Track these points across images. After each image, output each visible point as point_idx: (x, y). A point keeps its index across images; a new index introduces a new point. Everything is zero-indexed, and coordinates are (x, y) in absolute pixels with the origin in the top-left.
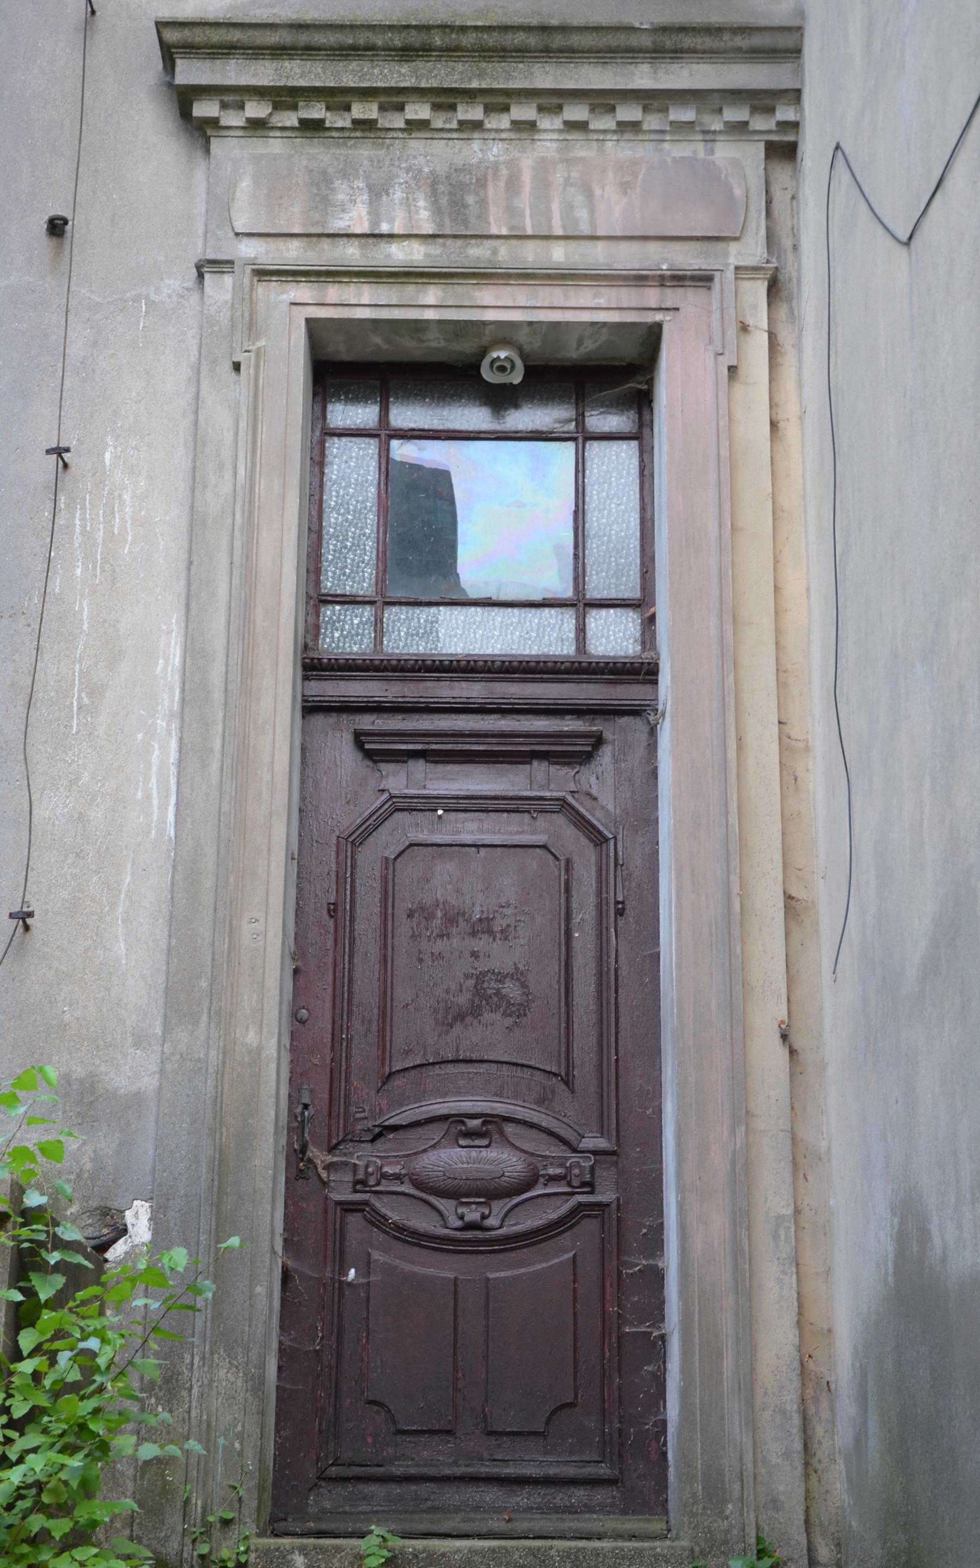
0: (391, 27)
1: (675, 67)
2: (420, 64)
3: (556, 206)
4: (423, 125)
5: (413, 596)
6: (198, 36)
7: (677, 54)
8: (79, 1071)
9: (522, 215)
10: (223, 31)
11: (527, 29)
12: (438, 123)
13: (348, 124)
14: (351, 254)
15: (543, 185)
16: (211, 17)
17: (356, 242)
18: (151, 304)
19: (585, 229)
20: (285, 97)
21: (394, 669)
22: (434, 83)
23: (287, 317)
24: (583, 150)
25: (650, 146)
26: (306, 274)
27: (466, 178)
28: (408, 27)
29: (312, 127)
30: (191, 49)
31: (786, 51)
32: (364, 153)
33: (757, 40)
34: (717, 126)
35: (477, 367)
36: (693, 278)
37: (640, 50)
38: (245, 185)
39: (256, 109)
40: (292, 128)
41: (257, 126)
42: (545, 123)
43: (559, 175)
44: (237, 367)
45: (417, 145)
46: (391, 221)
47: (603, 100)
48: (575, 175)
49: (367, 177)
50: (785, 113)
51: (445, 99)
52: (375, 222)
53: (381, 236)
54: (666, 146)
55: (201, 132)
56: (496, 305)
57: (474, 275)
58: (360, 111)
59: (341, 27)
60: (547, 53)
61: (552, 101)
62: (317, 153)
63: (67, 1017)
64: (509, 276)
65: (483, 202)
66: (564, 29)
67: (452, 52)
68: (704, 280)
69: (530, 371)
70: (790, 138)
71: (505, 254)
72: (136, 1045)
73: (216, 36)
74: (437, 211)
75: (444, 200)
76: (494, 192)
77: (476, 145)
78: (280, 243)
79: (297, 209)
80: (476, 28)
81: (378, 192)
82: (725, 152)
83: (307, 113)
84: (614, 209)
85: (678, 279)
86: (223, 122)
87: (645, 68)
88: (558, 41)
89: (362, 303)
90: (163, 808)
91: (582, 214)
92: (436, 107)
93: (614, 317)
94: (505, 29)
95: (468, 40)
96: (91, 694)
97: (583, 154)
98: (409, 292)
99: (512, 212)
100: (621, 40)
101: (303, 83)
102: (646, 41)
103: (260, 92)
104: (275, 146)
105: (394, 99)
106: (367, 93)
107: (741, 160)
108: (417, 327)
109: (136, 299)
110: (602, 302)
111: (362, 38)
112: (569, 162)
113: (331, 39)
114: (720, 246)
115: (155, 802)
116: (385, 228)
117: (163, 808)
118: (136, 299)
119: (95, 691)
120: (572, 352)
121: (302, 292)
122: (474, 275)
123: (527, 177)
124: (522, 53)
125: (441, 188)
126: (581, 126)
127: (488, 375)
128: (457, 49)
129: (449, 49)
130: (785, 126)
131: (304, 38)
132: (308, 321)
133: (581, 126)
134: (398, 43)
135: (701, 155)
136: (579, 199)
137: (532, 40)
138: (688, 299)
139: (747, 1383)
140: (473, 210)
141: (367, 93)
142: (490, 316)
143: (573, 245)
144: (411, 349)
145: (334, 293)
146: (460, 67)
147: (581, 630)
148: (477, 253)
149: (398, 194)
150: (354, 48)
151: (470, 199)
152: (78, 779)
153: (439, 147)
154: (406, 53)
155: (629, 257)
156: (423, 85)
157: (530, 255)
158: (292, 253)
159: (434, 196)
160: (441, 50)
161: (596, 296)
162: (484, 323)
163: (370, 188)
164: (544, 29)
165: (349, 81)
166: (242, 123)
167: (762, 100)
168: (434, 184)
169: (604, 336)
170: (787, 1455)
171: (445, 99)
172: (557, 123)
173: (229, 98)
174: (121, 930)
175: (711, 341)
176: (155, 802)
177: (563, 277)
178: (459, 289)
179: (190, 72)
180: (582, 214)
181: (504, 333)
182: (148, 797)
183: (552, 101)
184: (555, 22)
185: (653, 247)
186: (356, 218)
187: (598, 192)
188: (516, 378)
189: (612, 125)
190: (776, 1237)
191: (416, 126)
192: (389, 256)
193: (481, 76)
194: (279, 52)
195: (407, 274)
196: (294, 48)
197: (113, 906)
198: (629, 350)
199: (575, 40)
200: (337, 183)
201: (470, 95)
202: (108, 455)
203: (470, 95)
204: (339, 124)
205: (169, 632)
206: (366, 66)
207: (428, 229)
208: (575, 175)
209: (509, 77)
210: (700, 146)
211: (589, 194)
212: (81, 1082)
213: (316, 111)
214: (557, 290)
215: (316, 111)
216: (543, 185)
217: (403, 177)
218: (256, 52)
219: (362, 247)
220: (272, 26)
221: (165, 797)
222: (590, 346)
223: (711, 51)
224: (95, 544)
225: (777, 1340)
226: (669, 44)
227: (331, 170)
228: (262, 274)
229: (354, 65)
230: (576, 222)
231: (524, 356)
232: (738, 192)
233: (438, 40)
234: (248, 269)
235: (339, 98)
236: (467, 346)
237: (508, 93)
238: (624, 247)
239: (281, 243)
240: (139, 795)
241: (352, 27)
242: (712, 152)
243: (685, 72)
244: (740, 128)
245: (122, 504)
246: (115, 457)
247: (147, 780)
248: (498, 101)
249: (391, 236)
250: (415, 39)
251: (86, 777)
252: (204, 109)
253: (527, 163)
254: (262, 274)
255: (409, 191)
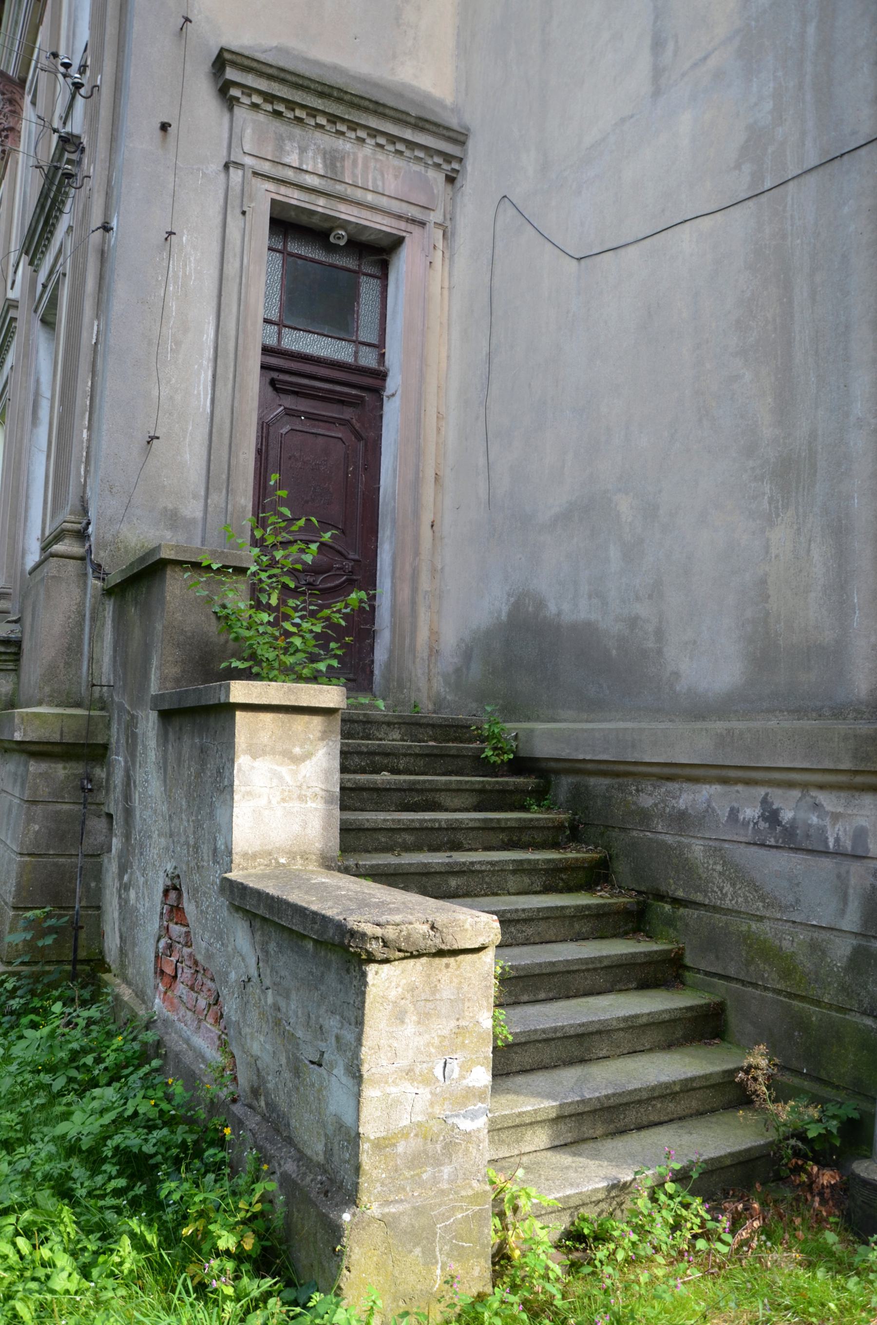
0: (318, 82)
1: (420, 134)
2: (326, 101)
3: (370, 177)
4: (322, 127)
5: (294, 325)
6: (239, 60)
7: (422, 129)
8: (170, 506)
9: (357, 177)
10: (250, 61)
11: (370, 101)
12: (328, 128)
13: (292, 117)
14: (290, 174)
15: (366, 167)
16: (233, 49)
17: (292, 170)
18: (204, 173)
19: (380, 190)
20: (270, 98)
21: (289, 355)
22: (331, 111)
23: (263, 196)
24: (381, 156)
25: (405, 162)
26: (273, 179)
27: (337, 155)
28: (325, 84)
29: (277, 114)
30: (234, 64)
31: (460, 142)
32: (297, 131)
33: (451, 134)
34: (430, 162)
35: (328, 236)
36: (419, 222)
37: (410, 123)
38: (249, 131)
39: (256, 99)
40: (269, 112)
41: (255, 106)
42: (368, 141)
43: (372, 164)
44: (244, 213)
45: (318, 134)
46: (307, 165)
47: (393, 139)
48: (378, 166)
49: (298, 143)
50: (455, 166)
51: (333, 119)
52: (301, 164)
53: (303, 170)
54: (411, 164)
55: (230, 103)
56: (346, 213)
57: (339, 198)
58: (299, 113)
59: (298, 76)
60: (375, 113)
61: (374, 133)
62: (276, 125)
63: (166, 483)
64: (352, 202)
65: (343, 167)
66: (384, 106)
67: (339, 100)
68: (422, 224)
69: (349, 241)
70: (454, 175)
71: (349, 191)
72: (194, 498)
73: (246, 62)
74: (325, 166)
75: (328, 162)
76: (348, 163)
77: (341, 142)
78: (262, 161)
79: (270, 148)
80: (351, 94)
81: (303, 150)
82: (431, 173)
83: (278, 108)
84: (391, 185)
85: (413, 221)
86: (241, 100)
87: (409, 131)
88: (381, 109)
89: (295, 197)
90: (205, 400)
91: (380, 183)
92: (328, 121)
93: (388, 230)
94: (362, 98)
95: (347, 97)
96: (175, 345)
97: (380, 158)
98: (313, 198)
99: (354, 175)
100: (404, 117)
101: (279, 94)
102: (413, 121)
103: (260, 92)
104: (261, 117)
105: (313, 112)
106: (303, 107)
107: (437, 178)
108: (313, 213)
109: (198, 170)
110: (385, 222)
111: (306, 83)
112: (377, 160)
113: (294, 79)
114: (428, 211)
115: (202, 396)
116: (304, 167)
117: (205, 400)
118: (198, 170)
119: (178, 343)
120: (364, 238)
121: (270, 186)
122: (339, 198)
123: (360, 161)
124: (366, 110)
125: (327, 156)
126: (381, 146)
127: (332, 239)
128: (342, 99)
129: (339, 99)
130: (454, 170)
131: (282, 75)
132: (272, 200)
133: (381, 146)
134: (319, 89)
135: (423, 172)
136: (379, 177)
137: (371, 106)
138: (416, 230)
139: (413, 649)
140: (339, 169)
141: (303, 107)
142: (343, 216)
143: (375, 195)
144: (304, 220)
145: (283, 190)
146: (341, 107)
147: (356, 353)
148: (339, 188)
149: (310, 154)
150: (302, 86)
151: (338, 164)
152: (170, 381)
153: (326, 138)
154: (322, 95)
155: (397, 207)
156: (327, 110)
157: (359, 194)
158: (266, 168)
159: (324, 159)
160: (335, 98)
161: (383, 219)
162: (339, 219)
163: (300, 148)
164: (376, 103)
165: (298, 99)
166: (249, 103)
167: (448, 158)
168: (325, 154)
169: (381, 235)
170: (423, 674)
171: (333, 119)
172: (373, 142)
173: (247, 91)
174: (187, 449)
175: (423, 249)
176: (202, 396)
177: (372, 208)
178: (332, 202)
179: (231, 74)
180: (380, 183)
181: (344, 224)
182: (199, 394)
183: (374, 133)
184: (381, 102)
185: (404, 205)
186: (293, 159)
187: (386, 176)
188: (342, 243)
189: (393, 149)
190: (425, 598)
191: (319, 126)
192: (305, 179)
193: (349, 114)
194: (270, 77)
195: (314, 190)
196: (277, 78)
197: (185, 438)
198: (385, 243)
199: (387, 111)
200: (286, 142)
201: (343, 120)
202: (184, 239)
203: (343, 120)
204: (289, 116)
205: (209, 323)
206: (305, 95)
207: (322, 172)
208: (378, 166)
209: (360, 118)
210: (423, 168)
211: (383, 176)
212: (171, 511)
213: (281, 108)
214: (369, 213)
215: (281, 108)
216: (366, 167)
217: (313, 147)
218: (261, 74)
219: (295, 172)
220: (271, 66)
221: (206, 395)
222: (372, 237)
223: (434, 133)
224: (178, 277)
225: (423, 635)
226: (420, 125)
227: (284, 135)
228: (255, 174)
229: (300, 93)
230: (377, 186)
231: (348, 234)
232: (435, 191)
233: (335, 94)
234: (251, 170)
235: (291, 105)
236: (327, 225)
237: (358, 124)
238: (394, 202)
239: (262, 162)
240: (196, 392)
241: (303, 77)
242: (427, 172)
243: (424, 137)
244: (438, 166)
245: (190, 262)
246: (187, 239)
247: (199, 386)
248: (354, 126)
249: (307, 171)
250: (326, 90)
251: (173, 381)
252: (235, 92)
253: (360, 155)
254: (255, 174)
255: (315, 154)
